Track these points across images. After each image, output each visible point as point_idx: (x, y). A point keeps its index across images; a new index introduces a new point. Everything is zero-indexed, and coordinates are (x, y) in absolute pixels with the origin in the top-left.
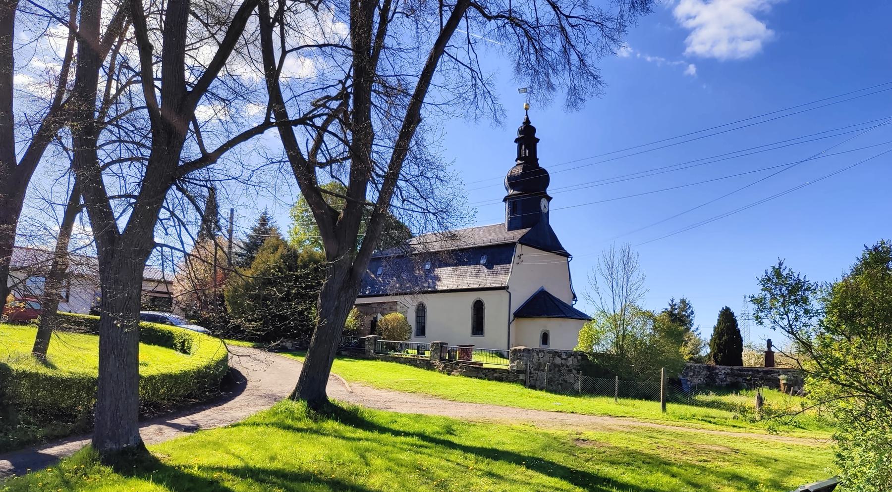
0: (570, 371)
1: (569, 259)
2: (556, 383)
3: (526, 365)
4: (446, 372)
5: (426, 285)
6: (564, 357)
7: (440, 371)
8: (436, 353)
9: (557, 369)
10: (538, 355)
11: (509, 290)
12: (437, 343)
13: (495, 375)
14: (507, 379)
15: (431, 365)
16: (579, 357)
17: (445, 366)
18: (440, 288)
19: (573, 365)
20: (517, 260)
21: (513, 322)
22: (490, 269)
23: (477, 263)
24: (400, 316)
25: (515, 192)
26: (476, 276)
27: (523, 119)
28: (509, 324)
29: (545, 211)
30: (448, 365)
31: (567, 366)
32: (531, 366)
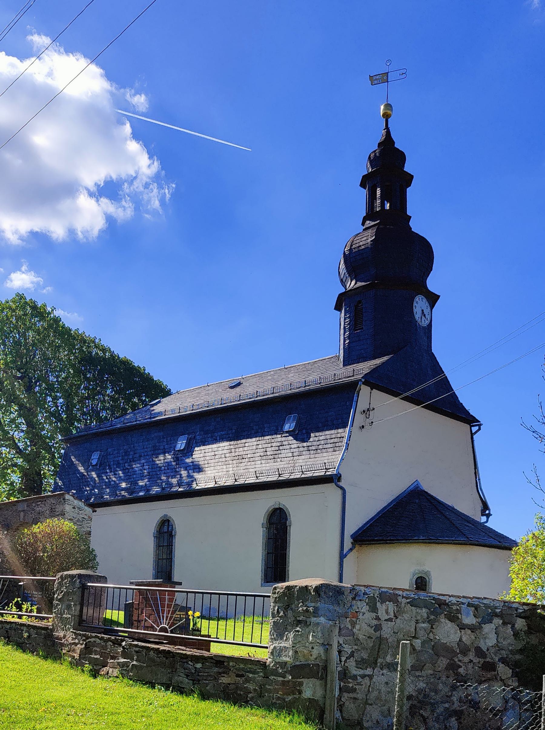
0: (489, 667)
1: (474, 429)
2: (440, 710)
3: (327, 646)
4: (87, 667)
5: (174, 481)
6: (469, 619)
7: (76, 664)
8: (69, 607)
9: (443, 662)
10: (374, 609)
11: (341, 484)
12: (72, 577)
13: (225, 680)
14: (261, 696)
15: (54, 644)
16: (520, 623)
17: (86, 647)
18: (202, 485)
19: (498, 647)
20: (359, 419)
21: (352, 554)
22: (303, 441)
23: (277, 430)
24: (67, 525)
25: (360, 284)
26: (274, 457)
27: (380, 135)
28: (342, 556)
29: (424, 323)
30: (94, 644)
31: (480, 652)
32: (348, 649)
